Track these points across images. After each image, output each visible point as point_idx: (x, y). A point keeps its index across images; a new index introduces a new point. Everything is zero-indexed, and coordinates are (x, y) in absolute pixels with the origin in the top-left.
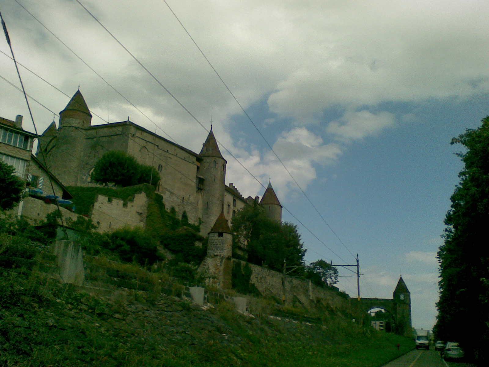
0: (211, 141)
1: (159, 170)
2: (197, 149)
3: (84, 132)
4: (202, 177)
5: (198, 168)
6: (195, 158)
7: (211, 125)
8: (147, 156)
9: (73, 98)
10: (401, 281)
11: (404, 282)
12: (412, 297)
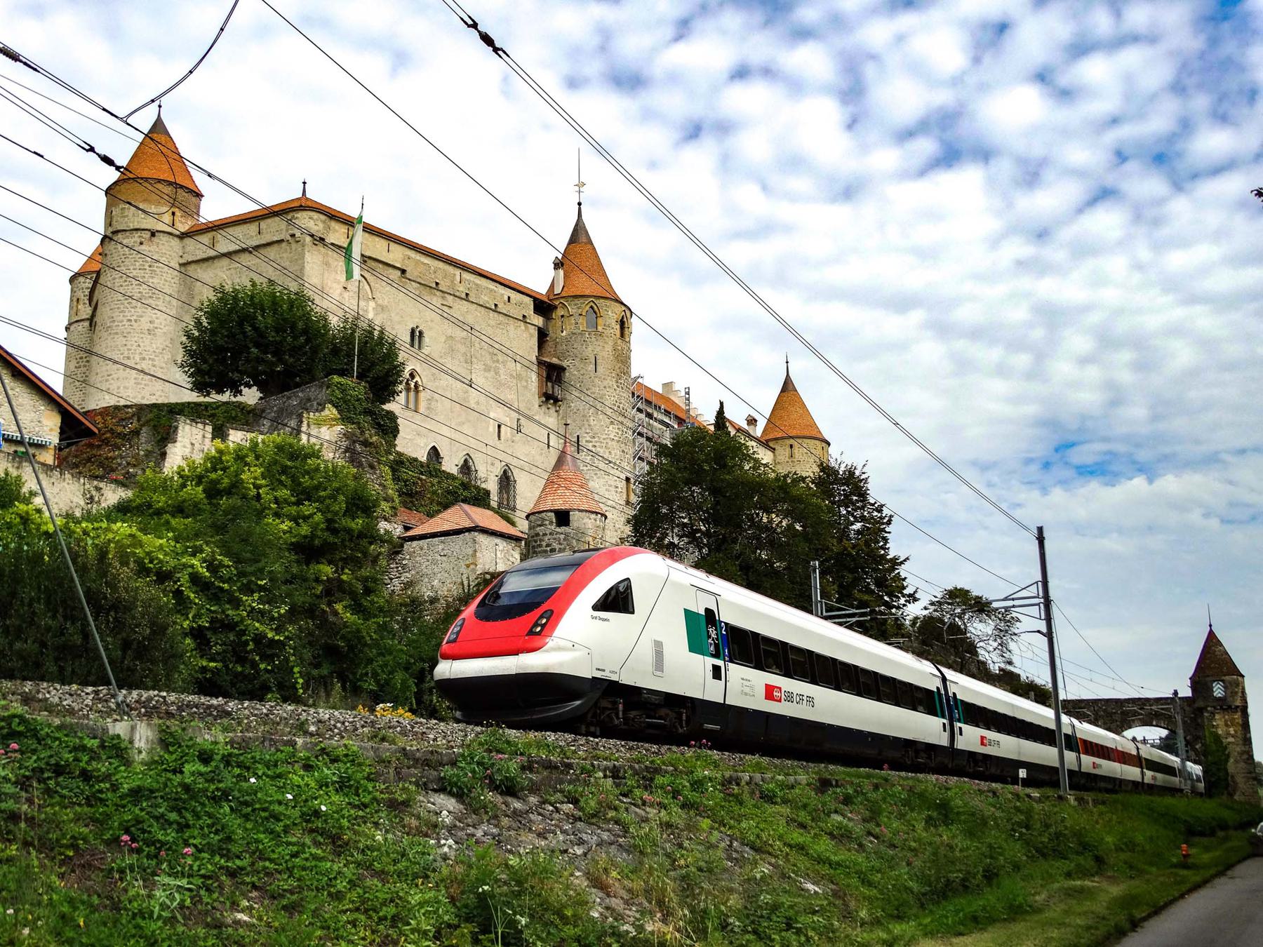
0: (578, 251)
1: (412, 345)
2: (541, 279)
3: (175, 242)
4: (555, 361)
5: (542, 335)
6: (529, 302)
7: (580, 204)
8: (372, 304)
9: (66, 370)
10: (1212, 641)
11: (1221, 645)
12: (1250, 686)
